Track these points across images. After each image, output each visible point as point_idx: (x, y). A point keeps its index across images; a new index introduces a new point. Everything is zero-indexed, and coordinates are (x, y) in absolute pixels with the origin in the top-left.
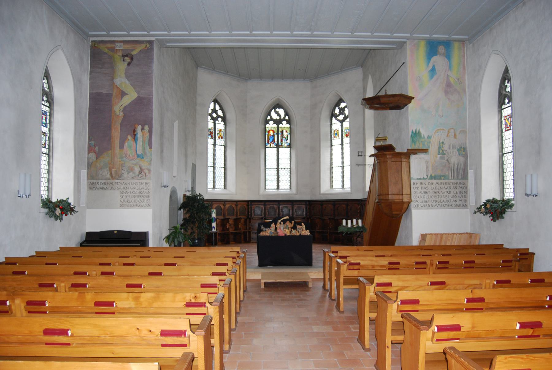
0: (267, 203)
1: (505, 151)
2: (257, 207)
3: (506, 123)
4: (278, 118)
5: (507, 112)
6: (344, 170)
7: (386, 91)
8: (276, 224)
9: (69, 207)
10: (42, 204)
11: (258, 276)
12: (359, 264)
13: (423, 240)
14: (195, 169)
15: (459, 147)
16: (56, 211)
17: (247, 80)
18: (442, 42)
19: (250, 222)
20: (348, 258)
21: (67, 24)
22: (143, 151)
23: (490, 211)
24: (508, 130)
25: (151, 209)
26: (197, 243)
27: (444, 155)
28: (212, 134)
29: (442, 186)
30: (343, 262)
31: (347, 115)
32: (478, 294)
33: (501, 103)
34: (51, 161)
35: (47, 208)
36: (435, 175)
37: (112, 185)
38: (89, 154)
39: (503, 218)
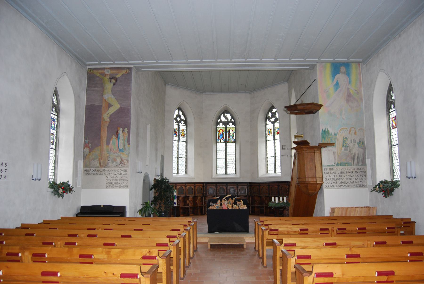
0: (218, 185)
1: (393, 143)
2: (210, 187)
3: (393, 122)
4: (226, 120)
5: (393, 114)
6: (276, 159)
7: (302, 100)
8: (221, 201)
9: (68, 188)
10: (49, 185)
11: (206, 240)
12: (277, 230)
13: (333, 212)
14: (164, 160)
15: (358, 142)
16: (59, 190)
17: (203, 93)
18: (343, 64)
19: (205, 199)
20: (269, 225)
21: (71, 57)
22: (123, 146)
23: (382, 190)
24: (394, 128)
25: (129, 190)
26: (164, 214)
27: (347, 148)
28: (177, 133)
29: (346, 171)
30: (265, 229)
31: (277, 117)
32: (356, 251)
33: (389, 108)
34: (57, 154)
35: (53, 188)
36: (341, 163)
37: (101, 171)
38: (85, 149)
39: (392, 195)
